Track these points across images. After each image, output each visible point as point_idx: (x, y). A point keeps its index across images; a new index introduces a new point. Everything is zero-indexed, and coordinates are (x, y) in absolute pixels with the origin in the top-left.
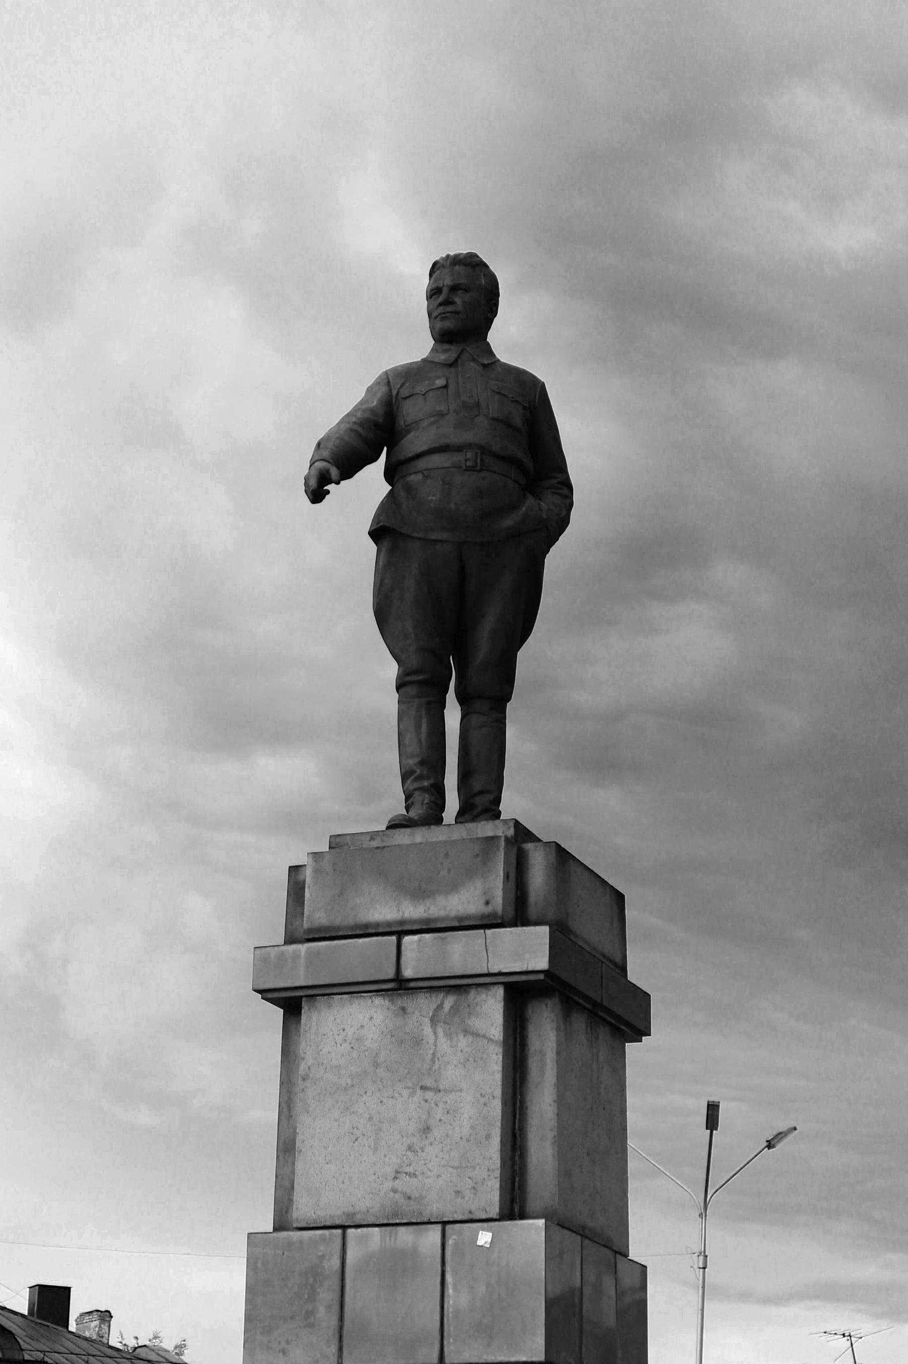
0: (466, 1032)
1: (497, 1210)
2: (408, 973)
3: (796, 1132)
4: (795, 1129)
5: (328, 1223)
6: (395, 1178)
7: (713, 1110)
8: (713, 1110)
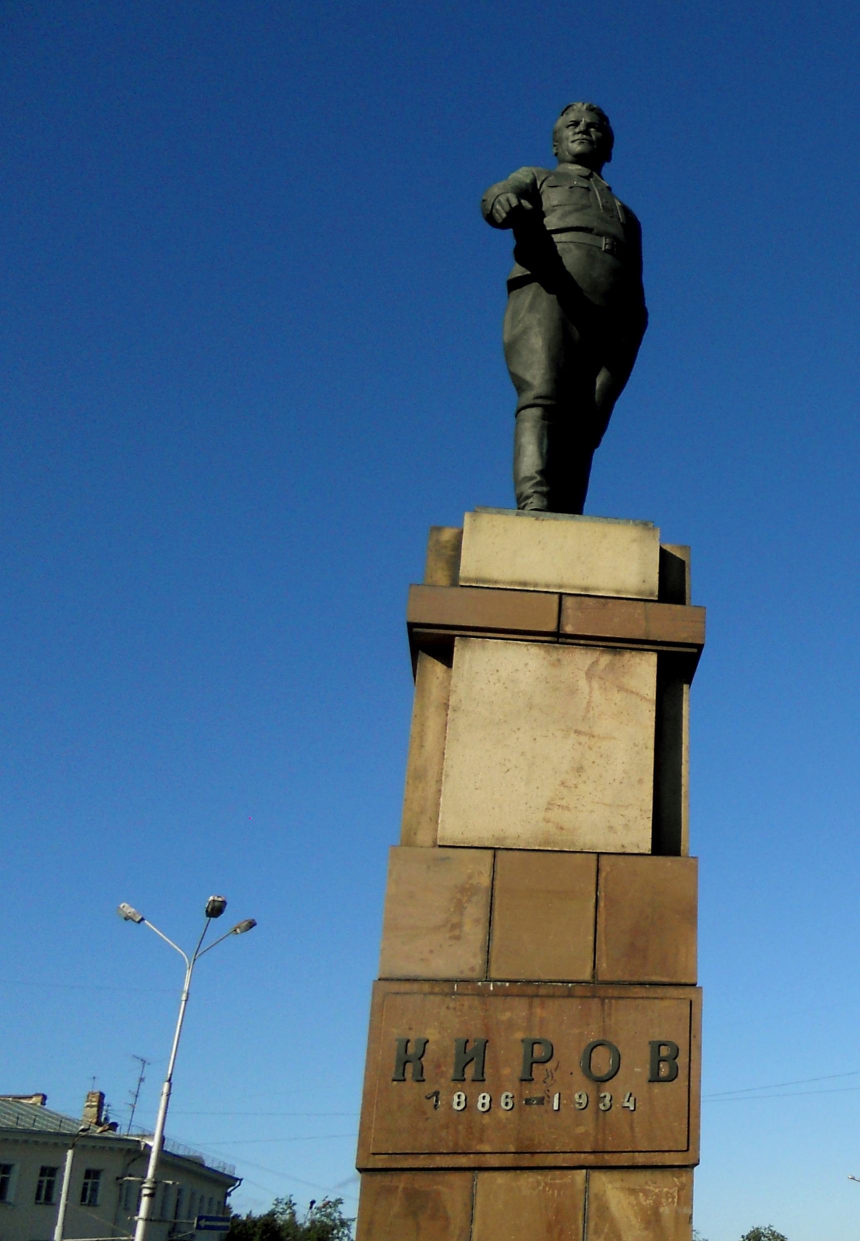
0: (621, 689)
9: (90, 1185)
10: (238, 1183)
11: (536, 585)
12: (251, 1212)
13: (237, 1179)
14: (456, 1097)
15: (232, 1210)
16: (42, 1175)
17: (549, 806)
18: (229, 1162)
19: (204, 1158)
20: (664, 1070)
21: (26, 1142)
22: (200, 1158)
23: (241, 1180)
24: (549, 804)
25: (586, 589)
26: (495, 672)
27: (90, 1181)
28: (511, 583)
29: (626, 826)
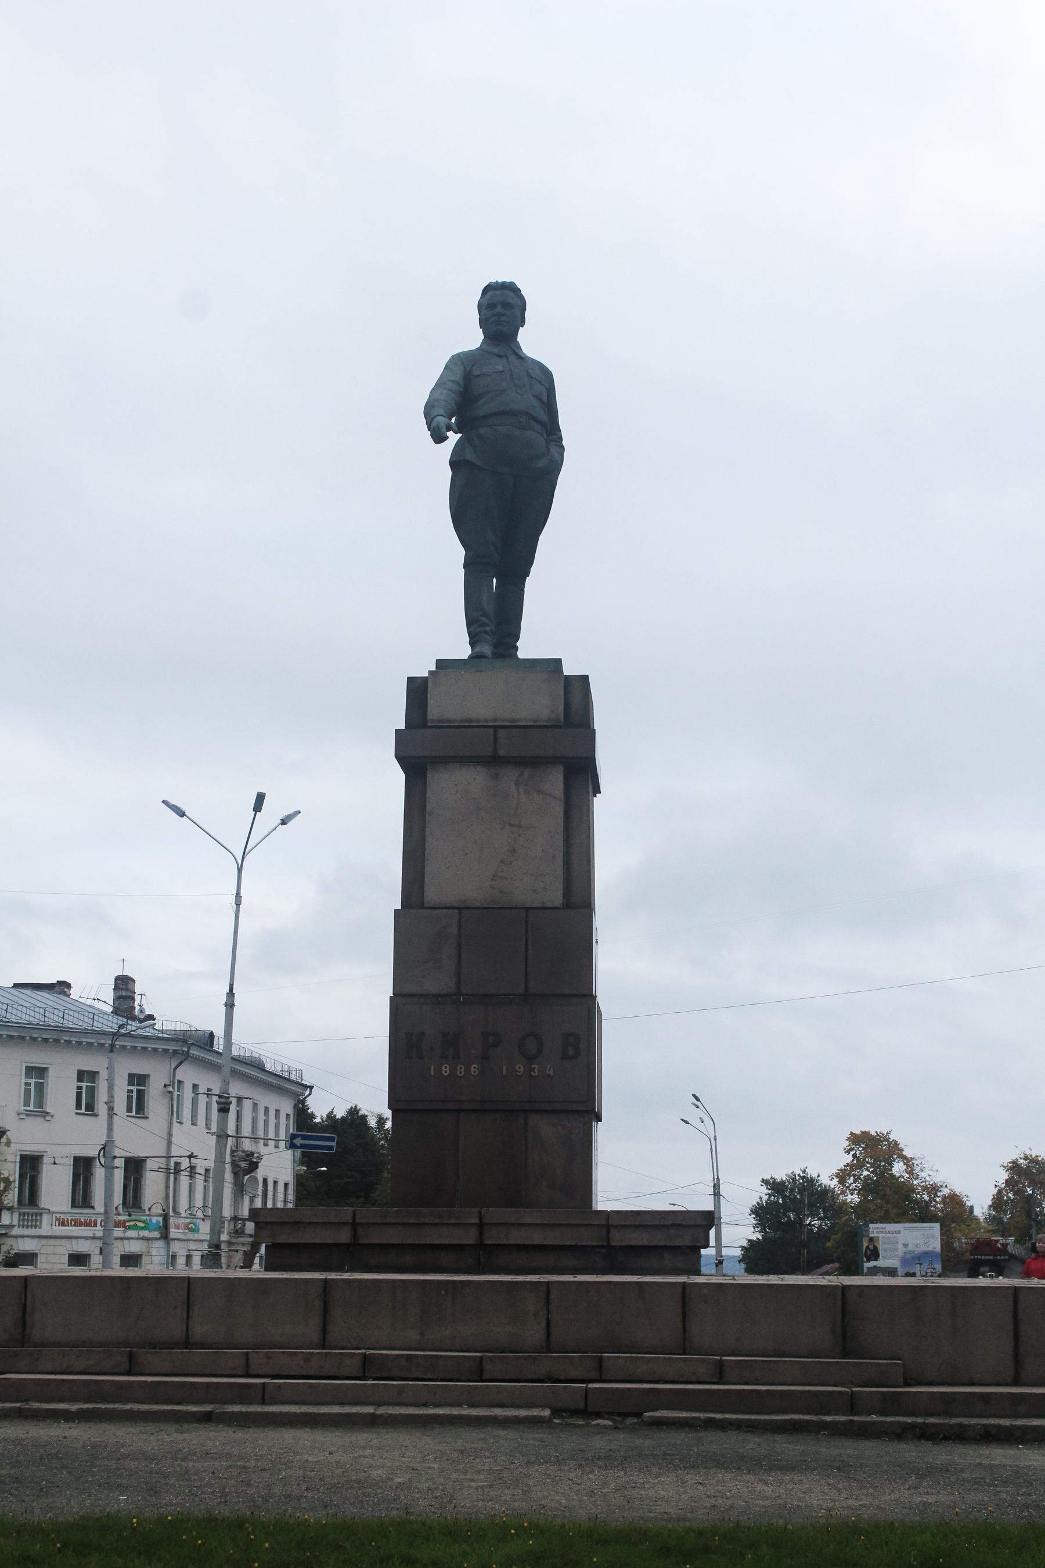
0: (540, 792)
1: (561, 902)
2: (502, 752)
3: (300, 814)
4: (300, 812)
5: (448, 905)
6: (493, 880)
7: (260, 798)
8: (260, 798)
9: (84, 1089)
10: (307, 1092)
11: (478, 721)
12: (332, 1112)
13: (306, 1087)
14: (443, 1068)
15: (361, 1113)
16: (80, 1079)
17: (494, 877)
18: (294, 1065)
19: (264, 1059)
20: (571, 1051)
21: (57, 1041)
22: (259, 1059)
23: (311, 1088)
24: (494, 876)
25: (513, 721)
26: (456, 784)
27: (84, 1085)
28: (462, 721)
29: (545, 889)
